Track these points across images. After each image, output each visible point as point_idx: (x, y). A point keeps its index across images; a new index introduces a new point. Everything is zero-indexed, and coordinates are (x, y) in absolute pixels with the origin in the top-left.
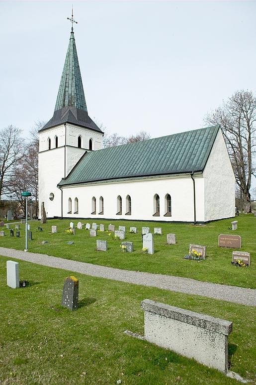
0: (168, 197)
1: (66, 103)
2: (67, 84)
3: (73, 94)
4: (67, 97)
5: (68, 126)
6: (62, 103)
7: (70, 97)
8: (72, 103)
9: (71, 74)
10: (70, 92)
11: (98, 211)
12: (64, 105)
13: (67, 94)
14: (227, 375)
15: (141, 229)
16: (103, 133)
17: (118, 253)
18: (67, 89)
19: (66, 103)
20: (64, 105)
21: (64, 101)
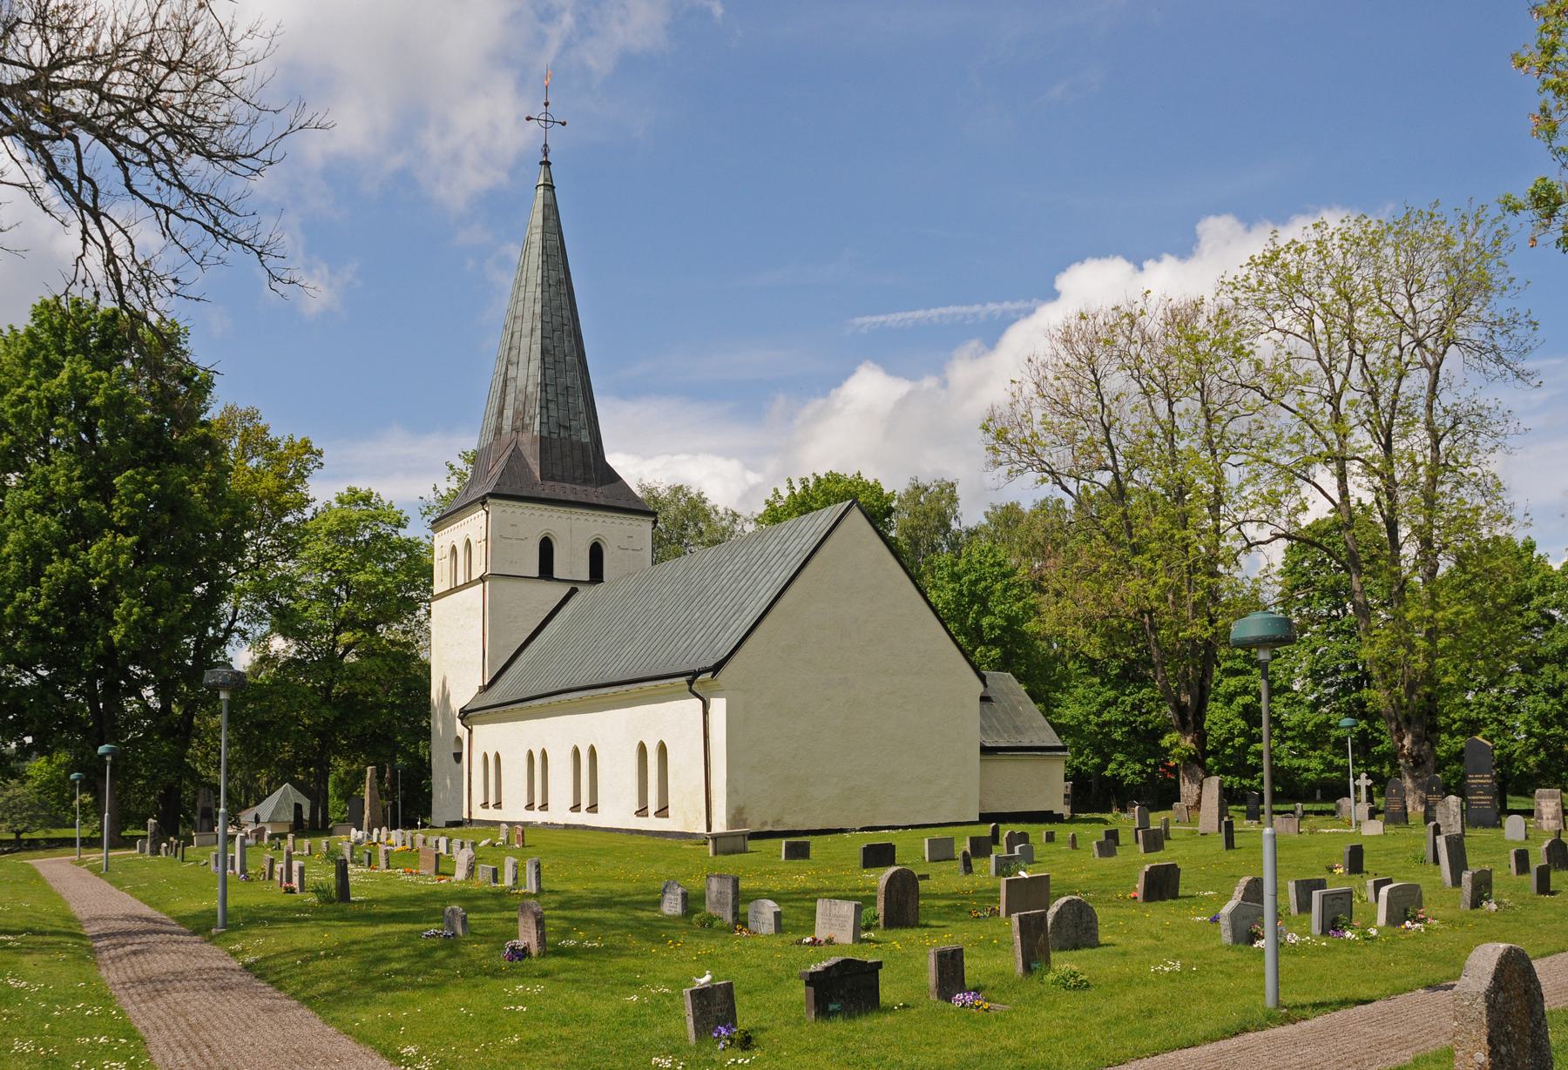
0: (662, 749)
1: (507, 425)
2: (514, 352)
3: (530, 389)
4: (510, 399)
5: (495, 506)
6: (493, 421)
7: (522, 397)
8: (527, 421)
9: (528, 316)
10: (521, 383)
11: (653, 806)
12: (498, 430)
13: (511, 389)
14: (1440, 646)
15: (812, 913)
16: (654, 514)
17: (88, 1027)
18: (512, 373)
19: (507, 425)
20: (498, 430)
21: (501, 413)
